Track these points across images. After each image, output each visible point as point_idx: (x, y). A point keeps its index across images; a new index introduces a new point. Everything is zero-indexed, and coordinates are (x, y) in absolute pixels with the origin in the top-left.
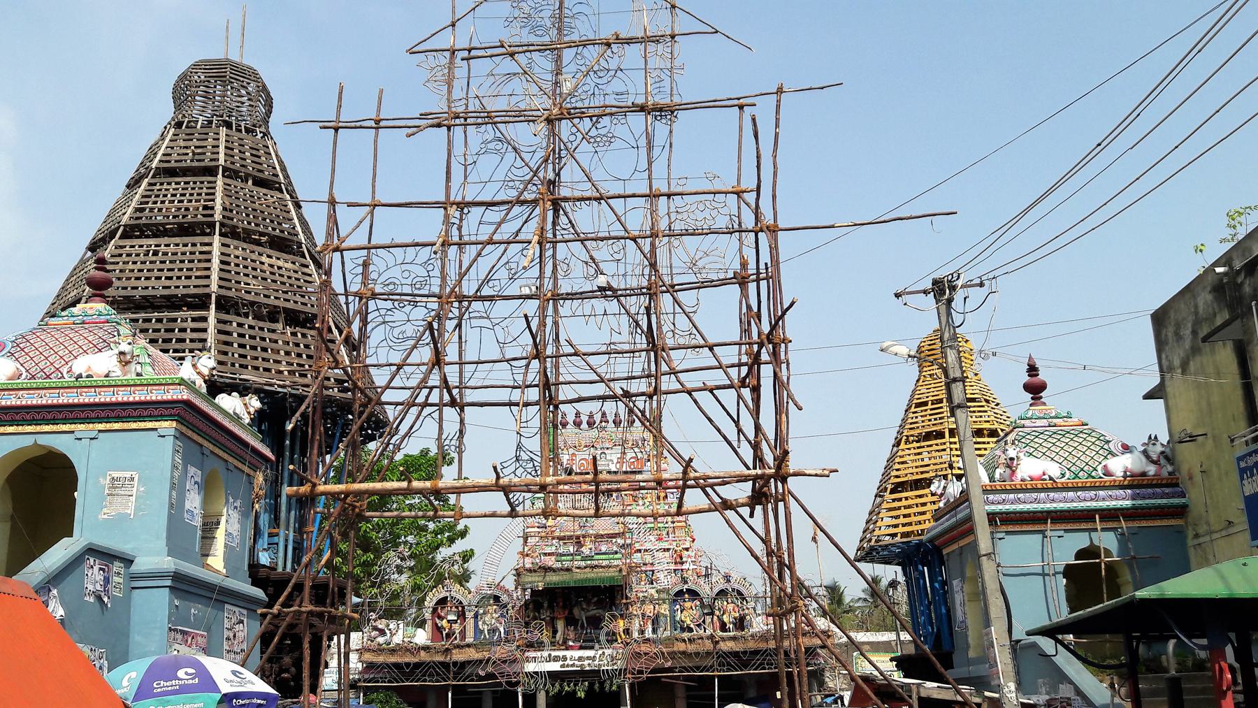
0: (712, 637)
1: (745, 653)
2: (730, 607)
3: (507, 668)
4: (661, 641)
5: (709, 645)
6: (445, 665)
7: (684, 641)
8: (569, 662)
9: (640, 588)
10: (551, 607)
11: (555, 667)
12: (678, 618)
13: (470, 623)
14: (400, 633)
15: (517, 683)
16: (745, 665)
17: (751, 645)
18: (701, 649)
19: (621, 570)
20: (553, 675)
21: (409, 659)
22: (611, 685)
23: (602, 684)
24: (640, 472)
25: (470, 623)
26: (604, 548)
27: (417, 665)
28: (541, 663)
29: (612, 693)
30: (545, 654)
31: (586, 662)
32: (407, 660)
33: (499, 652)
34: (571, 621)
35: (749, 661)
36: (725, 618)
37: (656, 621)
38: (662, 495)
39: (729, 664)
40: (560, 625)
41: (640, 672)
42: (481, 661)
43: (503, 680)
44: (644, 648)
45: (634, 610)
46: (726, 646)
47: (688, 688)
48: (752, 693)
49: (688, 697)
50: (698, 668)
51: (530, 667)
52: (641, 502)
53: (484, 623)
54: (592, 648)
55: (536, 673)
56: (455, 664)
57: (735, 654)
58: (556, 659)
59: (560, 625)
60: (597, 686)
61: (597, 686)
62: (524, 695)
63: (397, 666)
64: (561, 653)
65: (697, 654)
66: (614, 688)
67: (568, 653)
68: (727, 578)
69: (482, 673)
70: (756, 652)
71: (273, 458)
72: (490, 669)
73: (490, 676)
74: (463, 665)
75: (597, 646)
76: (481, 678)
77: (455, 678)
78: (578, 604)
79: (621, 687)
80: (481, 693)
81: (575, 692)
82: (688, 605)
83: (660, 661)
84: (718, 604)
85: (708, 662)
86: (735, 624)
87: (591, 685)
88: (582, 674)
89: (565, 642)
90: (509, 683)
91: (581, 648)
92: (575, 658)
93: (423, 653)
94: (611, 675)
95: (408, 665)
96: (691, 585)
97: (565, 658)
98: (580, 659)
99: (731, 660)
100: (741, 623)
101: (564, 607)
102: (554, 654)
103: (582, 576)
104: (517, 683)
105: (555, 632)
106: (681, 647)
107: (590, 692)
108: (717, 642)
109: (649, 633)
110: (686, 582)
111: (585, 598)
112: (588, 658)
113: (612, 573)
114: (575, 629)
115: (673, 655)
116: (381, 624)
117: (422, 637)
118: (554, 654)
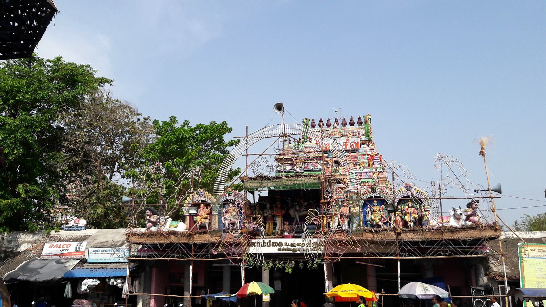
0: (395, 229)
1: (423, 242)
2: (411, 210)
3: (233, 250)
4: (353, 233)
5: (392, 236)
6: (188, 246)
7: (371, 232)
8: (284, 247)
9: (337, 193)
10: (271, 208)
11: (274, 250)
12: (369, 218)
13: (215, 219)
14: (168, 225)
15: (241, 260)
16: (424, 251)
17: (429, 236)
18: (385, 238)
19: (319, 178)
20: (268, 256)
21: (163, 241)
22: (312, 264)
23: (305, 263)
24: (357, 151)
25: (215, 219)
26: (311, 167)
27: (168, 246)
28: (261, 247)
29: (313, 270)
30: (261, 241)
31: (297, 247)
32: (161, 242)
33: (229, 237)
34: (287, 218)
35: (427, 249)
36: (407, 218)
37: (350, 218)
38: (371, 163)
39: (409, 250)
40: (279, 221)
41: (336, 255)
42: (214, 244)
43: (230, 258)
44: (339, 237)
45: (333, 209)
46: (408, 237)
47: (378, 270)
48: (430, 275)
49: (377, 276)
50: (383, 254)
51: (252, 250)
52: (358, 167)
53: (226, 219)
54: (300, 237)
55: (255, 254)
56: (195, 245)
57: (415, 243)
58: (275, 244)
59: (279, 221)
60: (301, 265)
61: (301, 265)
62: (246, 270)
63: (155, 246)
64: (278, 241)
65: (382, 243)
66: (315, 266)
67: (284, 241)
68: (408, 188)
69: (215, 252)
70: (432, 242)
71: (443, 293)
72: (220, 249)
73: (221, 255)
74: (203, 246)
75: (303, 235)
76: (213, 256)
77: (195, 256)
78: (293, 206)
79: (321, 266)
80: (221, 268)
81: (284, 268)
82: (376, 208)
83: (352, 247)
84: (401, 207)
85: (392, 249)
86: (415, 223)
87: (297, 263)
88: (294, 256)
89: (282, 233)
90: (234, 260)
91: (294, 237)
92: (288, 244)
93: (173, 237)
94: (313, 257)
95: (161, 245)
96: (378, 193)
97: (281, 244)
98: (292, 245)
99: (412, 248)
100: (419, 221)
101: (282, 208)
102: (273, 240)
103: (290, 183)
104: (241, 260)
105: (275, 225)
106: (369, 236)
107: (296, 268)
108: (399, 234)
109: (345, 227)
110: (374, 191)
111: (299, 203)
112: (298, 244)
113: (313, 180)
114: (290, 224)
115: (362, 243)
116: (153, 219)
117: (182, 227)
118: (273, 240)
